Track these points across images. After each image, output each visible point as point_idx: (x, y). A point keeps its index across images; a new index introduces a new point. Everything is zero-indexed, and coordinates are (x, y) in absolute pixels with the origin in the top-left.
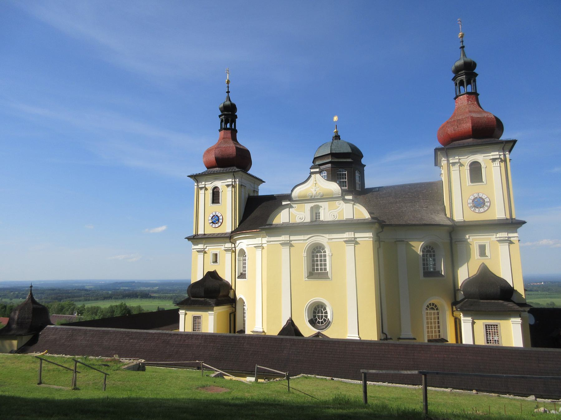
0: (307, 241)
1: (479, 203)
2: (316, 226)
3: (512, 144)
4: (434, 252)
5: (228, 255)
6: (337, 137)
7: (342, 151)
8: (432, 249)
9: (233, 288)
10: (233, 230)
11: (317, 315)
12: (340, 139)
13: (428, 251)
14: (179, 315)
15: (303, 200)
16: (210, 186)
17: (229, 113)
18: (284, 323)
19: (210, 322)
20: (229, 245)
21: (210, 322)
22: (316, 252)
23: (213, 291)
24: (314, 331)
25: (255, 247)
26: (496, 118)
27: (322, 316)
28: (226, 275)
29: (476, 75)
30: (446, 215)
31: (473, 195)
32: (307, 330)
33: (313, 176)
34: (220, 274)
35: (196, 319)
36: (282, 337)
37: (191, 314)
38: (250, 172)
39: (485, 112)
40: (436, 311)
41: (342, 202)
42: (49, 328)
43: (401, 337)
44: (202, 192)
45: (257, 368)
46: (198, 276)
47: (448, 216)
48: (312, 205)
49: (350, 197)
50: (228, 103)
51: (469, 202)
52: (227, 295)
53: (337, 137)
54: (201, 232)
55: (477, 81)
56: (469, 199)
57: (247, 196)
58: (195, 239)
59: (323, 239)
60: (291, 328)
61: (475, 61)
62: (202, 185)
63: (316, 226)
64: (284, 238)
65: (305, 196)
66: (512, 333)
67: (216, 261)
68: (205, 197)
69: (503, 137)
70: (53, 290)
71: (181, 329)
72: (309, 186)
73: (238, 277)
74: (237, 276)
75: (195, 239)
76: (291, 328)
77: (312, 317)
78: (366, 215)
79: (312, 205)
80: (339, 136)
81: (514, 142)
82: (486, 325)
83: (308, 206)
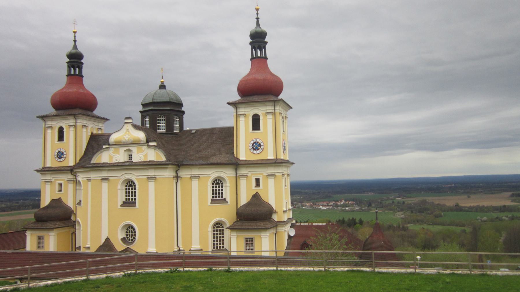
0: (121, 177)
1: (256, 146)
2: (130, 165)
5: (270, 117)
6: (162, 87)
9: (75, 212)
14: (26, 236)
15: (119, 144)
16: (56, 124)
18: (103, 241)
19: (52, 242)
21: (52, 242)
22: (130, 184)
24: (124, 247)
28: (70, 203)
29: (266, 43)
31: (253, 140)
32: (120, 246)
33: (126, 125)
34: (64, 200)
36: (286, 257)
40: (221, 229)
41: (146, 147)
43: (192, 249)
44: (49, 131)
47: (235, 156)
49: (155, 144)
50: (74, 51)
54: (49, 165)
56: (253, 140)
59: (134, 176)
60: (108, 245)
64: (105, 174)
65: (121, 142)
67: (60, 191)
68: (52, 135)
71: (29, 248)
76: (108, 245)
77: (125, 236)
78: (163, 159)
80: (165, 86)
83: (122, 150)
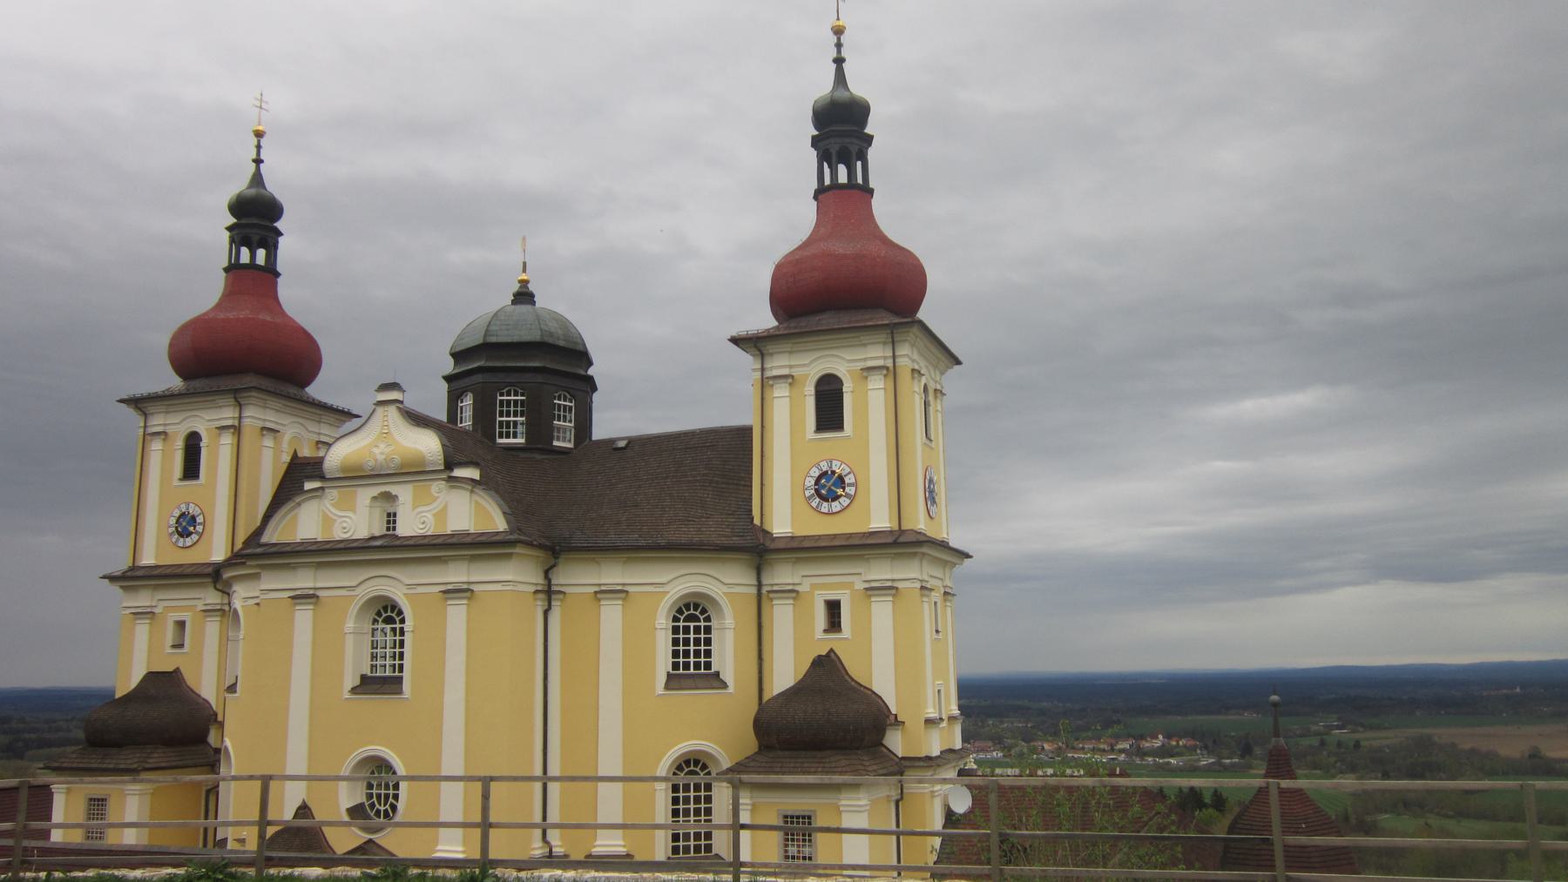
0: (358, 591)
2: (389, 548)
4: (708, 619)
5: (213, 627)
8: (704, 611)
9: (220, 718)
10: (239, 545)
12: (534, 303)
15: (356, 476)
17: (841, 128)
20: (212, 597)
23: (165, 729)
25: (293, 598)
27: (387, 796)
31: (817, 465)
33: (380, 410)
34: (190, 679)
35: (97, 805)
42: (405, 766)
45: (1286, 847)
46: (129, 679)
48: (375, 491)
49: (473, 473)
52: (202, 739)
54: (148, 559)
57: (287, 458)
58: (133, 577)
59: (399, 584)
62: (157, 422)
63: (389, 548)
64: (304, 580)
65: (360, 468)
68: (164, 460)
72: (366, 442)
75: (133, 577)
79: (375, 491)
80: (532, 296)
83: (365, 495)
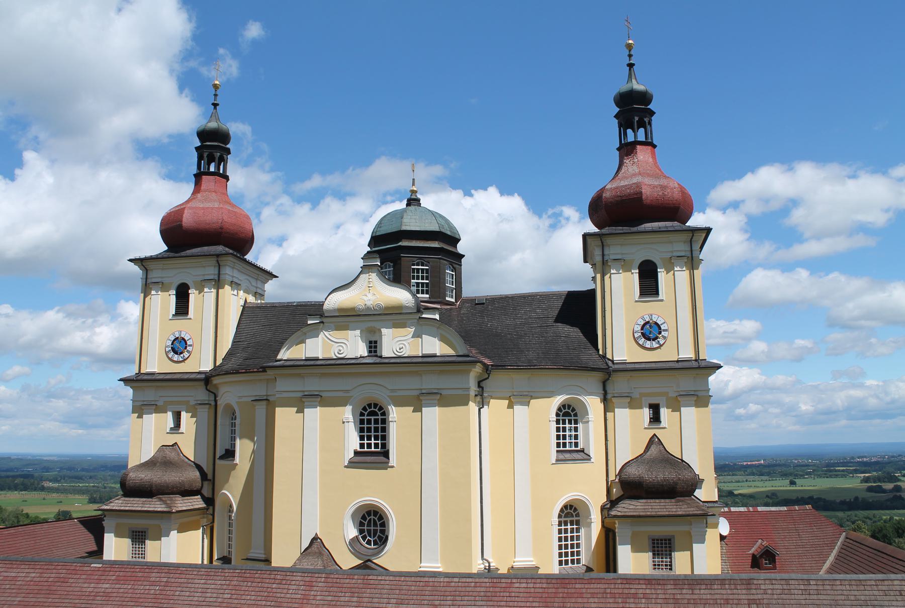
3: (704, 235)
7: (423, 229)
11: (373, 524)
12: (419, 205)
13: (567, 414)
26: (681, 187)
29: (652, 113)
30: (598, 350)
37: (683, 356)
38: (249, 257)
39: (665, 177)
51: (636, 329)
53: (413, 201)
55: (653, 123)
61: (651, 90)
66: (437, 317)
69: (692, 223)
70: (21, 459)
73: (221, 458)
74: (218, 456)
81: (708, 231)
82: (653, 540)
